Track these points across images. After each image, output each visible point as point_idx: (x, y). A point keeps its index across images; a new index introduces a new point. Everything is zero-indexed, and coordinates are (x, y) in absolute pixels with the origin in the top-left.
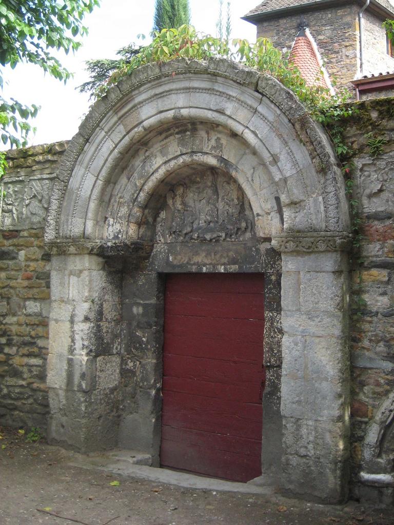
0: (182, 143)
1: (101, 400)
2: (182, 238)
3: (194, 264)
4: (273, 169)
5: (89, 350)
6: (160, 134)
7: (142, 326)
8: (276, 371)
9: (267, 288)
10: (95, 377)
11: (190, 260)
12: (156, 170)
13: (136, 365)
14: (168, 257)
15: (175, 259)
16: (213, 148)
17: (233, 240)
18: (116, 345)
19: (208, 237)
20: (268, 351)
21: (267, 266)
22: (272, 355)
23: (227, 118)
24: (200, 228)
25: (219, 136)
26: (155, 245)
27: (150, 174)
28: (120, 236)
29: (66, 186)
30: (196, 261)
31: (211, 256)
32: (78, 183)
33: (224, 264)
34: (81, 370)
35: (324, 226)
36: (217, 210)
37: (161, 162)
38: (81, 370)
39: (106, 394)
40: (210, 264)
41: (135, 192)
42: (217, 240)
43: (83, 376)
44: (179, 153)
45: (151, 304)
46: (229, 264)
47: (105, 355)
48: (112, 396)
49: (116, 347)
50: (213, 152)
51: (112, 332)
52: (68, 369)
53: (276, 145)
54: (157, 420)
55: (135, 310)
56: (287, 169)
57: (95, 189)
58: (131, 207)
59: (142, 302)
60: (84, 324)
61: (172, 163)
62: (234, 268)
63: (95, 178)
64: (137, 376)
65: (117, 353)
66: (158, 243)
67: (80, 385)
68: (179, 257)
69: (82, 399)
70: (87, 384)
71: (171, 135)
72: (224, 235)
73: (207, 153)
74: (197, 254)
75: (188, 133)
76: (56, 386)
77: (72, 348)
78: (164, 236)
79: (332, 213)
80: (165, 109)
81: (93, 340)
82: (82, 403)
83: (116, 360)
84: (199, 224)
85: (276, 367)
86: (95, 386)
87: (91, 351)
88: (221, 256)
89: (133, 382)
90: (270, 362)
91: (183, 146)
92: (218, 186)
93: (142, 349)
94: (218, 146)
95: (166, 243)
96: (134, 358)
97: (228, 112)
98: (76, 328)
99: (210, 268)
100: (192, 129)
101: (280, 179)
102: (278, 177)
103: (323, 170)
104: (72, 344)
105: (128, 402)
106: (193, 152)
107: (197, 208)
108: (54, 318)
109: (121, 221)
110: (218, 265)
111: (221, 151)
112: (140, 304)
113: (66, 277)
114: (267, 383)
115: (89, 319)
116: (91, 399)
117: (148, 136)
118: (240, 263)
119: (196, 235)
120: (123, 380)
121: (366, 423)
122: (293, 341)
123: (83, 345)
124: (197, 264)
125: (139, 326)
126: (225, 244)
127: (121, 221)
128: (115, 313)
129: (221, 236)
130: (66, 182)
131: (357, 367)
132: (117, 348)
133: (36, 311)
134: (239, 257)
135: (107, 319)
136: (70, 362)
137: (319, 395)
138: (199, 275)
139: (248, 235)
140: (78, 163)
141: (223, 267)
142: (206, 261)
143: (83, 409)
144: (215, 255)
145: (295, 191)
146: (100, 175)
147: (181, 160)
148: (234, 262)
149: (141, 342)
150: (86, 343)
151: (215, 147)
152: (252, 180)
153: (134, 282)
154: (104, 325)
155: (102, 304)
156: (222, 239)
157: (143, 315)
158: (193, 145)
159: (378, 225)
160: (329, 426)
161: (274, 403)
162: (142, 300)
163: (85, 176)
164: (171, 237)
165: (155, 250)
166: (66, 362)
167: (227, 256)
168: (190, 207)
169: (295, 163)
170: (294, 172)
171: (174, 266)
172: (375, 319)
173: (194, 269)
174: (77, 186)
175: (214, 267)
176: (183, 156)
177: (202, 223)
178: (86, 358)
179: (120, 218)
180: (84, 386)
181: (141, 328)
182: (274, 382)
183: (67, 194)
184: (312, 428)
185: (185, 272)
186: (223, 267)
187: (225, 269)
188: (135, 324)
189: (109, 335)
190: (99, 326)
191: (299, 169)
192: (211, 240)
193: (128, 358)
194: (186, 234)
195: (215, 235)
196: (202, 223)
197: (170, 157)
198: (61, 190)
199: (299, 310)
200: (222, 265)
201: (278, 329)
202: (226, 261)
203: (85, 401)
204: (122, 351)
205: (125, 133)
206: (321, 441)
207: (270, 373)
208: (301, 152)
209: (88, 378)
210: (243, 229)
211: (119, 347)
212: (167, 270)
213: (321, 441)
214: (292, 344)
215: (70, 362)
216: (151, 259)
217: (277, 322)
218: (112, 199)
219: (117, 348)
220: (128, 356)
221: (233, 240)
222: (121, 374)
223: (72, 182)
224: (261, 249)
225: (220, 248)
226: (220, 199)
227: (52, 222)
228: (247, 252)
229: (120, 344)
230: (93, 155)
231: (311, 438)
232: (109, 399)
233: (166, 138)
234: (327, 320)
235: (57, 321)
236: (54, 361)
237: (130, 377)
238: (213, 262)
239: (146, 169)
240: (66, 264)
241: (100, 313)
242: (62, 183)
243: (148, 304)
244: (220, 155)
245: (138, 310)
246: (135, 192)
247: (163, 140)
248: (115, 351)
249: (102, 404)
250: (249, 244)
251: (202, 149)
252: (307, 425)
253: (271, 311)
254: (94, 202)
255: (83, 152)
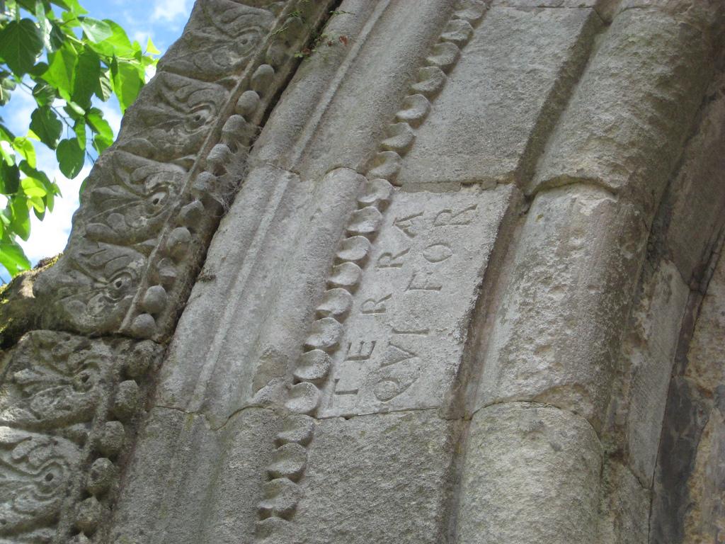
29: (147, 376)
32: (289, 305)
57: (510, 305)
63: (493, 205)
130: (136, 338)
140: (267, 150)
146: (567, 123)
163: (365, 227)
174: (278, 337)
183: (149, 451)
198: (87, 416)
218: (699, 433)
223: (211, 321)
230: (431, 42)
242: (101, 348)
254: (534, 432)
255: (321, 51)
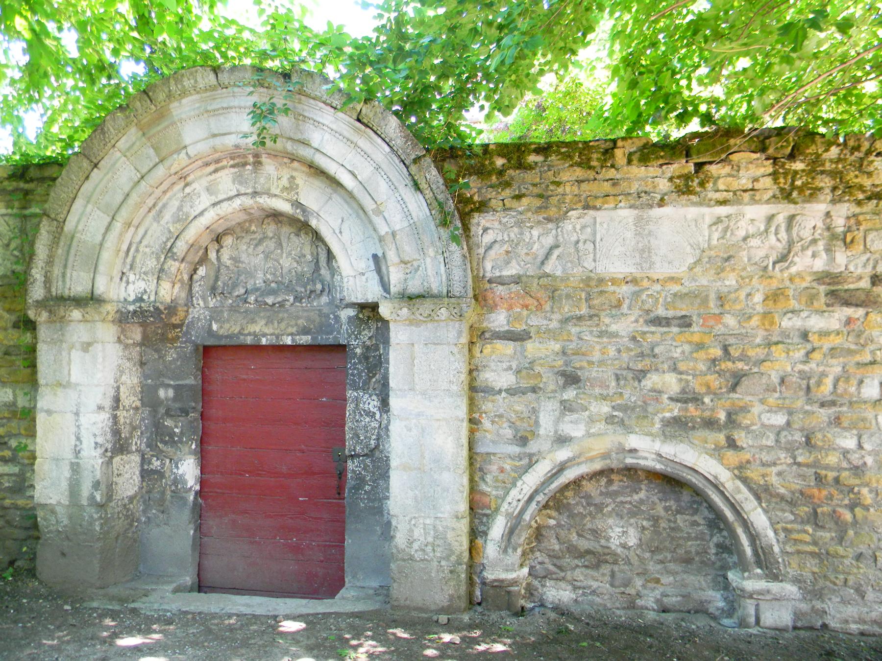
0: (239, 179)
1: (118, 513)
2: (230, 301)
3: (249, 334)
4: (378, 221)
5: (103, 449)
6: (207, 164)
7: (172, 413)
8: (362, 461)
9: (350, 362)
10: (112, 485)
11: (243, 329)
12: (201, 214)
13: (164, 464)
14: (210, 325)
15: (221, 327)
16: (285, 189)
17: (304, 305)
18: (135, 440)
19: (270, 300)
20: (352, 438)
21: (350, 336)
22: (357, 442)
23: (313, 151)
24: (257, 289)
25: (295, 174)
26: (190, 310)
27: (190, 219)
28: (145, 297)
30: (252, 331)
31: (273, 324)
33: (292, 334)
34: (94, 477)
35: (445, 291)
36: (282, 268)
37: (208, 204)
38: (94, 477)
39: (125, 505)
40: (271, 335)
41: (168, 240)
42: (282, 304)
43: (96, 485)
44: (234, 193)
45: (186, 385)
46: (298, 334)
47: (122, 454)
48: (131, 506)
49: (137, 442)
50: (285, 194)
51: (131, 424)
52: (70, 478)
53: (382, 189)
54: (195, 531)
55: (162, 393)
56: (398, 222)
58: (162, 259)
59: (172, 383)
60: (96, 415)
61: (225, 205)
62: (305, 339)
63: (109, 219)
64: (165, 478)
65: (137, 450)
66: (195, 308)
67: (92, 498)
68: (227, 326)
69: (96, 516)
70: (102, 495)
71: (223, 168)
72: (292, 299)
73: (275, 195)
74: (253, 321)
75: (248, 167)
76: (53, 502)
77: (78, 449)
78: (204, 299)
79: (457, 274)
80: (221, 132)
81: (109, 436)
82: (95, 520)
83: (136, 458)
84: (255, 284)
85: (363, 456)
86: (112, 496)
87: (106, 451)
88: (288, 325)
89: (159, 486)
90: (354, 450)
91: (241, 183)
92: (282, 238)
93: (175, 442)
94: (292, 187)
95: (207, 307)
96: (160, 454)
97: (315, 144)
98: (83, 420)
99: (272, 340)
100: (254, 163)
101: (387, 233)
102: (383, 229)
103: (444, 224)
104: (78, 443)
105: (154, 511)
106: (255, 194)
107: (252, 264)
108: (45, 408)
109: (145, 278)
110: (283, 335)
111: (297, 193)
112: (169, 386)
113: (64, 353)
114: (349, 475)
115: (103, 408)
116: (107, 514)
117: (190, 167)
118: (314, 333)
119: (252, 298)
120: (144, 484)
121: (487, 515)
122: (405, 426)
123: (96, 443)
124: (255, 335)
125: (168, 414)
126: (293, 309)
127: (145, 278)
128: (133, 398)
129: (288, 301)
131: (477, 454)
132: (136, 444)
133: (7, 400)
134: (312, 326)
135: (124, 407)
136: (75, 468)
137: (439, 488)
138: (257, 348)
139: (324, 299)
141: (290, 338)
142: (266, 331)
143: (98, 528)
144: (279, 323)
145: (407, 248)
147: (237, 202)
148: (305, 331)
149: (172, 435)
150: (100, 440)
151: (287, 188)
152: (341, 232)
153: (160, 357)
154: (122, 414)
155: (118, 388)
156: (289, 303)
157: (175, 399)
158: (255, 183)
159: (500, 290)
160: (453, 523)
161: (361, 499)
162: (172, 379)
164: (214, 300)
165: (191, 316)
166: (69, 467)
167: (296, 324)
168: (243, 262)
169: (408, 215)
170: (406, 224)
171: (222, 337)
172: (498, 397)
173: (249, 340)
175: (277, 337)
176: (242, 197)
177: (259, 283)
178: (100, 461)
179: (145, 273)
180: (98, 498)
181: (172, 416)
182: (360, 473)
184: (431, 527)
185: (236, 344)
186: (290, 338)
187: (293, 340)
188: (162, 410)
189: (128, 428)
190: (115, 417)
191: (412, 221)
192: (274, 304)
193: (152, 456)
194: (238, 296)
195: (279, 299)
196: (259, 283)
197: (221, 197)
199: (412, 389)
200: (288, 335)
201: (364, 411)
202: (294, 330)
203: (101, 518)
204: (143, 446)
205: (157, 160)
206: (442, 541)
207: (353, 463)
208: (416, 202)
209: (103, 487)
210: (318, 292)
211: (139, 442)
212: (210, 342)
213: (442, 541)
214: (405, 430)
215: (75, 468)
216: (184, 328)
217: (364, 403)
219: (136, 444)
220: (151, 453)
221: (304, 305)
222: (142, 477)
224: (342, 317)
225: (286, 315)
226: (284, 255)
227: (38, 276)
228: (323, 319)
229: (140, 437)
231: (430, 539)
232: (128, 511)
233: (216, 171)
234: (448, 400)
235: (49, 412)
236: (46, 467)
237: (156, 480)
238: (276, 332)
239: (185, 210)
240: (63, 335)
241: (117, 400)
243: (182, 385)
244: (294, 198)
245: (166, 393)
246: (168, 240)
247: (210, 174)
248: (134, 448)
249: (119, 518)
250: (326, 310)
251: (269, 189)
252: (424, 524)
253: (356, 390)
